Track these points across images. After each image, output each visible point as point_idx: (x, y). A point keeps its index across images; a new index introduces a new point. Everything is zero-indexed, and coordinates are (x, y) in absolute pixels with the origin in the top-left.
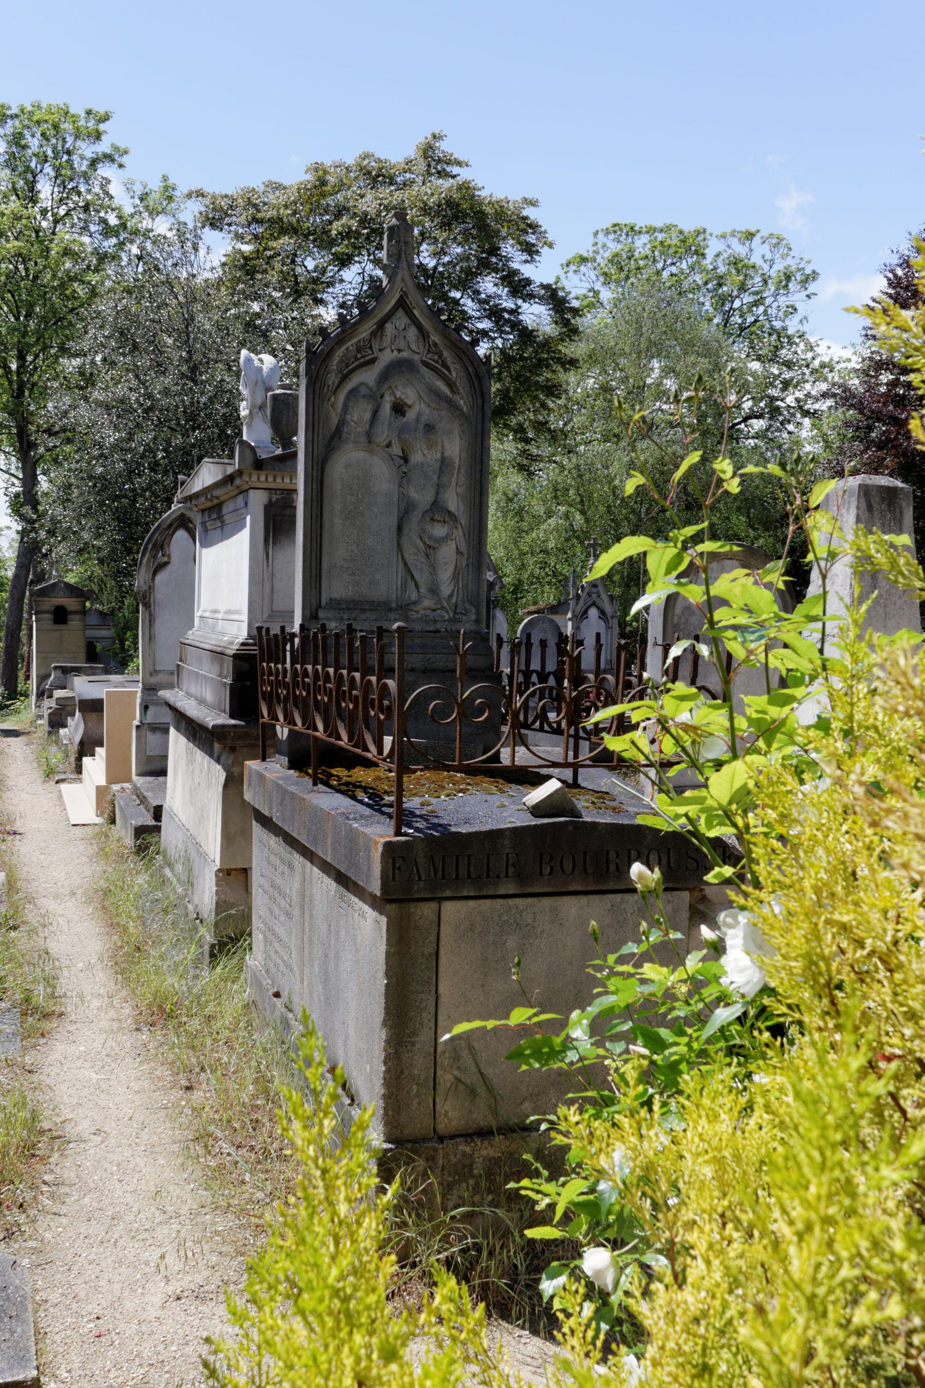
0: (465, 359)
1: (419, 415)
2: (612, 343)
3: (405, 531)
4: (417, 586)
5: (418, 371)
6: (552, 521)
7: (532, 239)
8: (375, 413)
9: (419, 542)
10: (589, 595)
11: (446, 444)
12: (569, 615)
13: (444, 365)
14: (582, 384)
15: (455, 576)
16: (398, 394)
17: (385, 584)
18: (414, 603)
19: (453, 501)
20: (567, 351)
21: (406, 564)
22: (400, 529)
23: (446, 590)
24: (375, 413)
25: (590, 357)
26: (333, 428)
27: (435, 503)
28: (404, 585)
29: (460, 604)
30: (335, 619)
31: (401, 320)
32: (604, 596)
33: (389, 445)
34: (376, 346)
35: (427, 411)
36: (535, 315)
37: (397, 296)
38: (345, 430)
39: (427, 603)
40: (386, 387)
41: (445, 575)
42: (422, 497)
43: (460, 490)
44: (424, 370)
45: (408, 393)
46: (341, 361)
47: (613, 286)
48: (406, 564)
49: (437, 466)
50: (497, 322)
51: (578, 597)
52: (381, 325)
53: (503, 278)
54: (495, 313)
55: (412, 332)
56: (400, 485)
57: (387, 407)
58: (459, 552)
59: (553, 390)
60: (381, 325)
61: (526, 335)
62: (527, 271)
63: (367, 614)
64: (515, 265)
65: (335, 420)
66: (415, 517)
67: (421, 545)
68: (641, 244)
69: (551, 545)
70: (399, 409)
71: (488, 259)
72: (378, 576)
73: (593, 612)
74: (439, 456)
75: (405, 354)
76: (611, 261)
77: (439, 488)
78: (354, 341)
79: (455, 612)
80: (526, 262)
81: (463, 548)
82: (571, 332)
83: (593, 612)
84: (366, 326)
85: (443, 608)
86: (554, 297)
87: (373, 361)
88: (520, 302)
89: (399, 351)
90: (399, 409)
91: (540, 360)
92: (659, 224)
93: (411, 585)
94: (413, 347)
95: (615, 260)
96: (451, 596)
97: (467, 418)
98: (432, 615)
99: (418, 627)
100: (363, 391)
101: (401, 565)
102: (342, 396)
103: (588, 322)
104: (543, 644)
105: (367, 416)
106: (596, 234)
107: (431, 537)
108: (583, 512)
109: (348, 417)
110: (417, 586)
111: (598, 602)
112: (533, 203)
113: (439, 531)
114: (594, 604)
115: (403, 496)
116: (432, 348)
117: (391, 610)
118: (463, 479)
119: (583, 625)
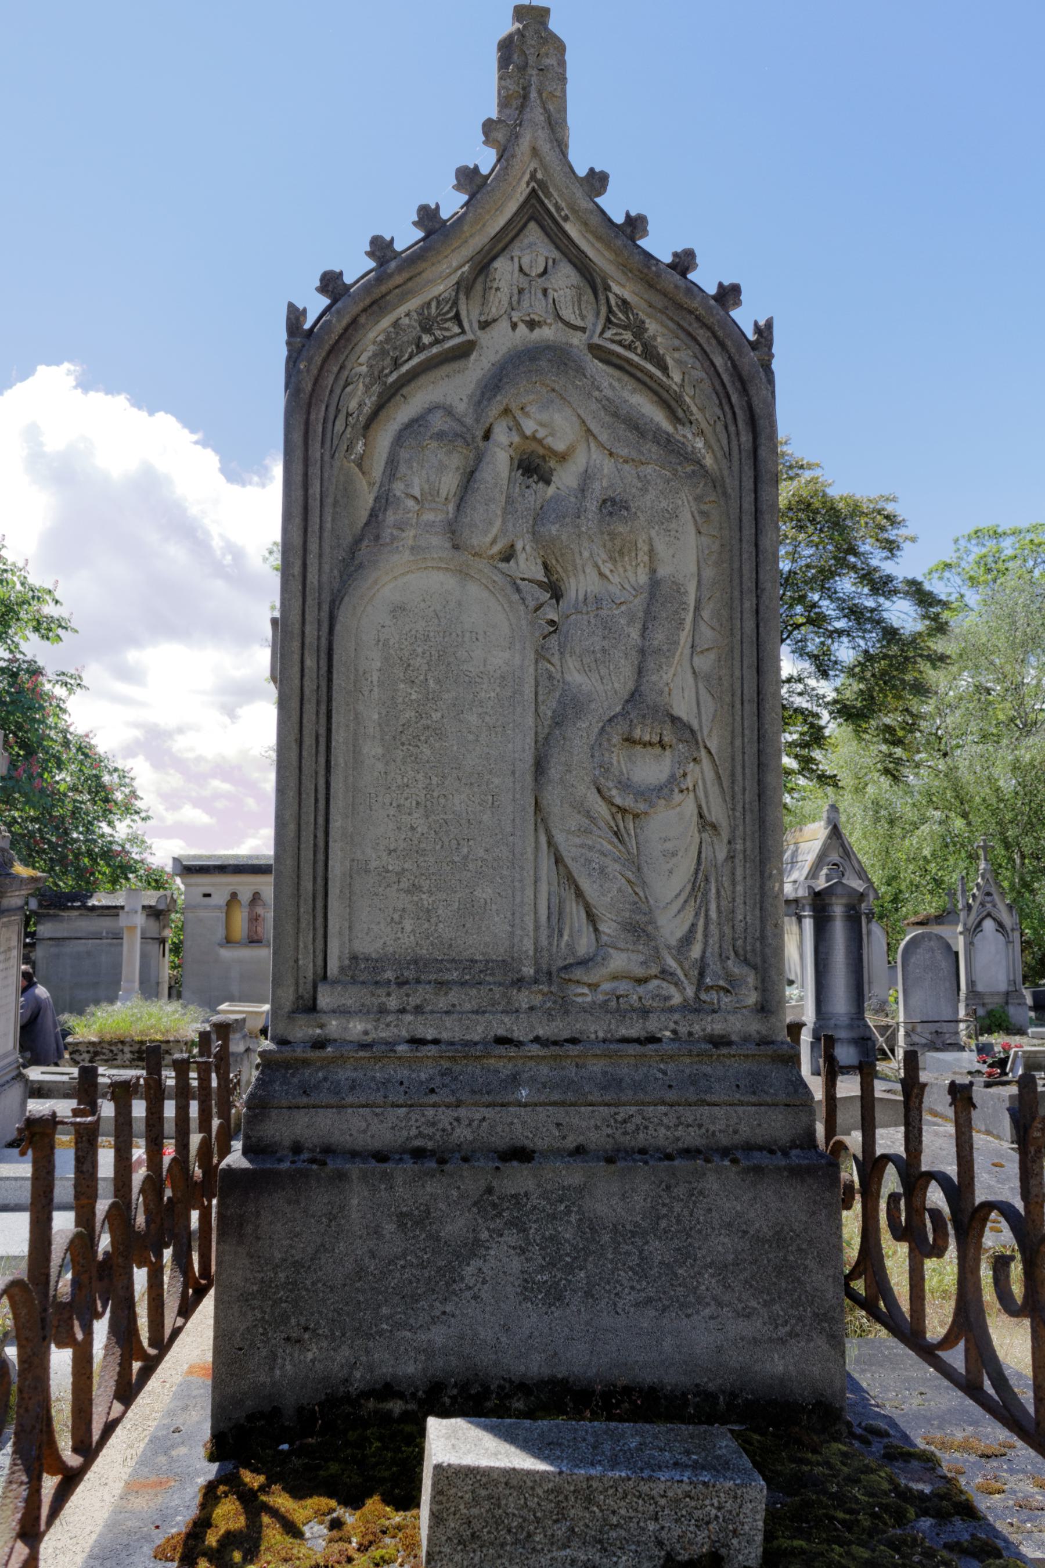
0: (702, 334)
1: (587, 477)
2: (984, 640)
3: (554, 772)
4: (592, 918)
5: (580, 371)
6: (925, 828)
7: (892, 534)
8: (469, 477)
9: (593, 797)
10: (982, 904)
11: (660, 547)
12: (960, 928)
13: (650, 353)
14: (952, 684)
15: (698, 886)
16: (529, 426)
17: (504, 915)
18: (584, 963)
19: (683, 690)
20: (933, 647)
21: (558, 860)
22: (540, 767)
23: (671, 926)
24: (469, 477)
25: (961, 655)
26: (364, 515)
27: (634, 697)
28: (557, 917)
29: (714, 966)
30: (363, 1012)
31: (534, 249)
32: (1001, 906)
33: (508, 555)
34: (470, 312)
35: (608, 466)
36: (902, 614)
37: (522, 192)
38: (391, 517)
39: (618, 961)
40: (494, 410)
41: (669, 885)
42: (603, 686)
43: (704, 663)
44: (596, 367)
45: (555, 424)
46: (382, 353)
47: (981, 588)
48: (558, 860)
49: (638, 603)
50: (857, 619)
51: (969, 907)
52: (482, 266)
53: (863, 577)
54: (855, 613)
55: (565, 280)
56: (541, 655)
57: (500, 460)
58: (705, 823)
59: (921, 689)
60: (482, 266)
61: (891, 634)
62: (888, 568)
63: (454, 996)
64: (874, 562)
65: (366, 499)
66: (581, 735)
67: (602, 809)
68: (1008, 547)
69: (926, 852)
70: (533, 466)
71: (845, 553)
72: (484, 893)
73: (989, 925)
74: (643, 578)
75: (547, 333)
76: (978, 563)
77: (644, 657)
78: (413, 304)
79: (700, 985)
80: (887, 558)
81: (717, 813)
82: (940, 628)
83: (989, 925)
84: (444, 267)
85: (665, 974)
86: (921, 596)
87: (464, 351)
88: (881, 600)
89: (532, 325)
90: (533, 466)
91: (907, 659)
92: (1024, 525)
93: (575, 913)
94: (568, 314)
95: (981, 561)
96: (687, 940)
97: (715, 483)
98: (635, 995)
99: (596, 1028)
100: (438, 422)
101: (546, 863)
102: (384, 438)
103: (958, 623)
104: (961, 1096)
105: (449, 483)
106: (956, 541)
107: (625, 786)
108: (964, 815)
109: (398, 488)
110: (592, 918)
111: (994, 913)
112: (894, 500)
113: (650, 769)
114: (989, 915)
115: (545, 681)
116: (617, 315)
117: (519, 983)
118: (707, 634)
119: (977, 940)
